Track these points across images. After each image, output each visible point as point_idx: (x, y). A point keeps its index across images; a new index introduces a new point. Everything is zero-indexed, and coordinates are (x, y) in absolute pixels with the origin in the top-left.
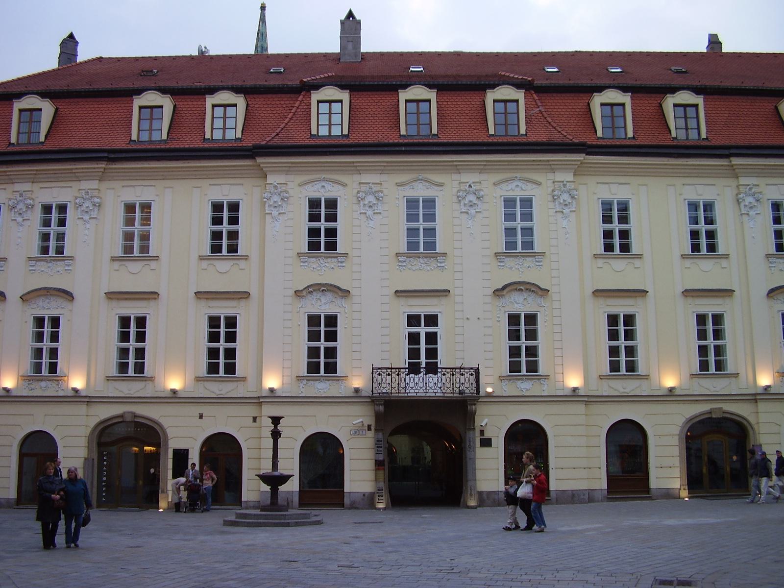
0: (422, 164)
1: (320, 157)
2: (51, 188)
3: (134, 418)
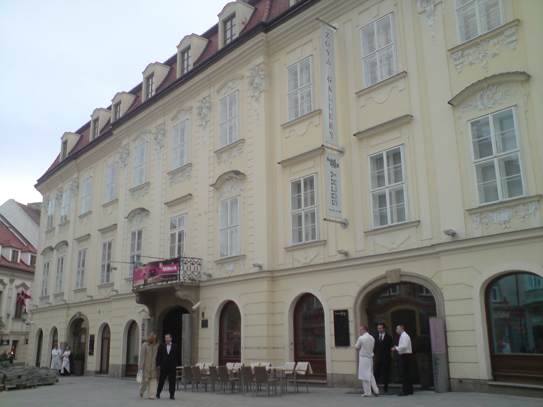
0: (284, 36)
1: (127, 123)
2: (368, 9)
3: (400, 278)
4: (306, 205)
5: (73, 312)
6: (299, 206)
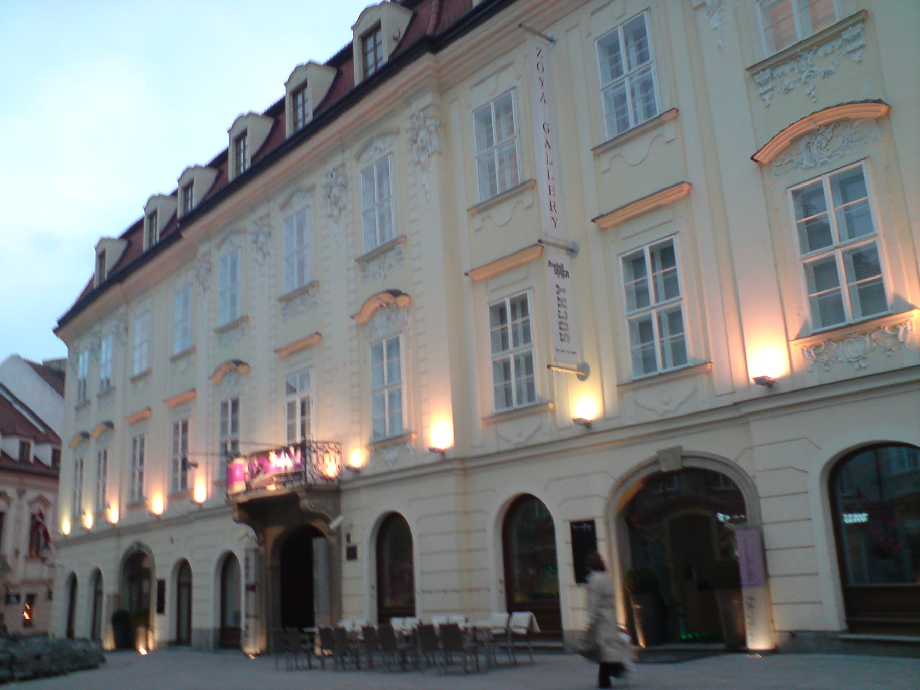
4: (516, 343)
5: (127, 543)
6: (505, 346)
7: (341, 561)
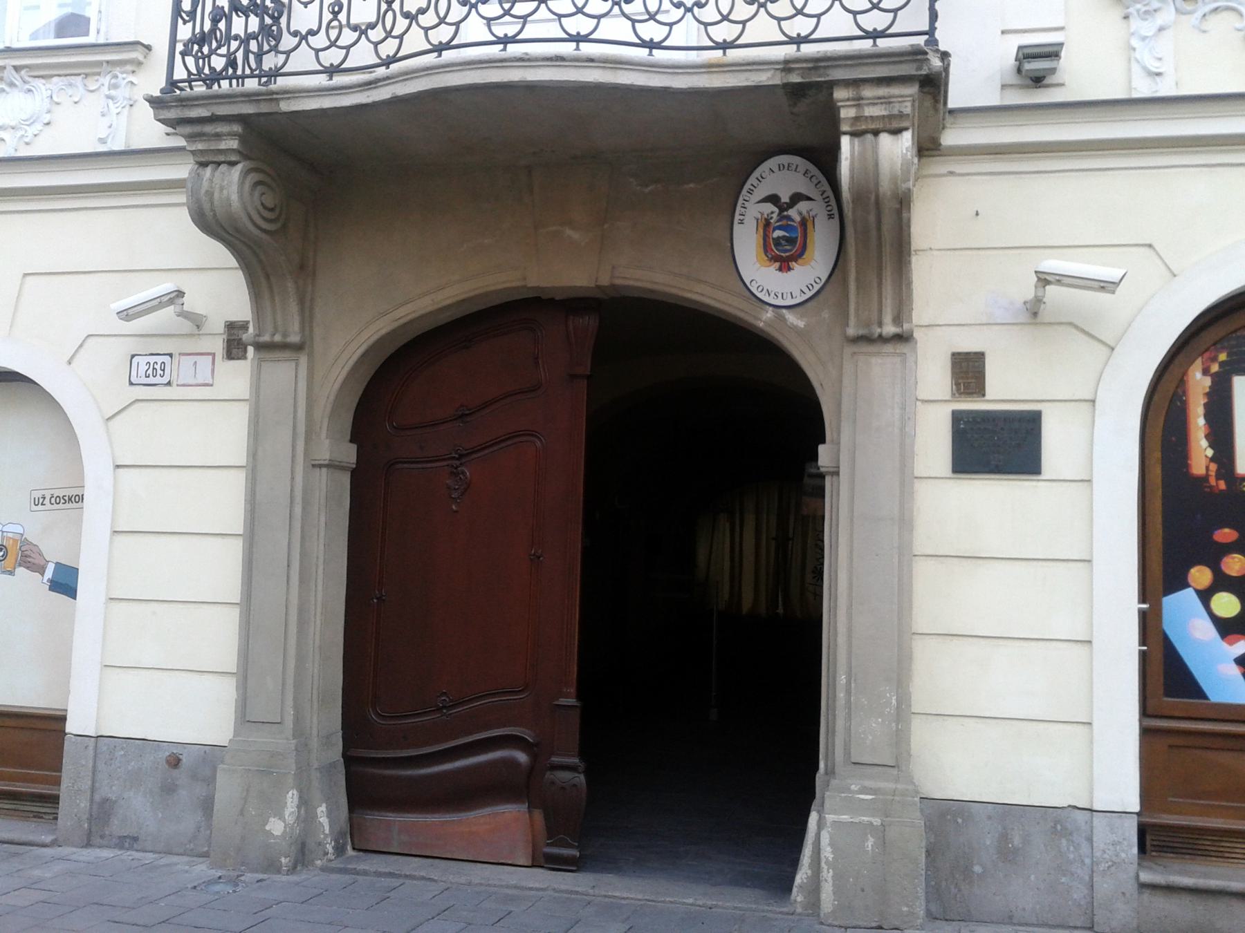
7: (906, 480)
